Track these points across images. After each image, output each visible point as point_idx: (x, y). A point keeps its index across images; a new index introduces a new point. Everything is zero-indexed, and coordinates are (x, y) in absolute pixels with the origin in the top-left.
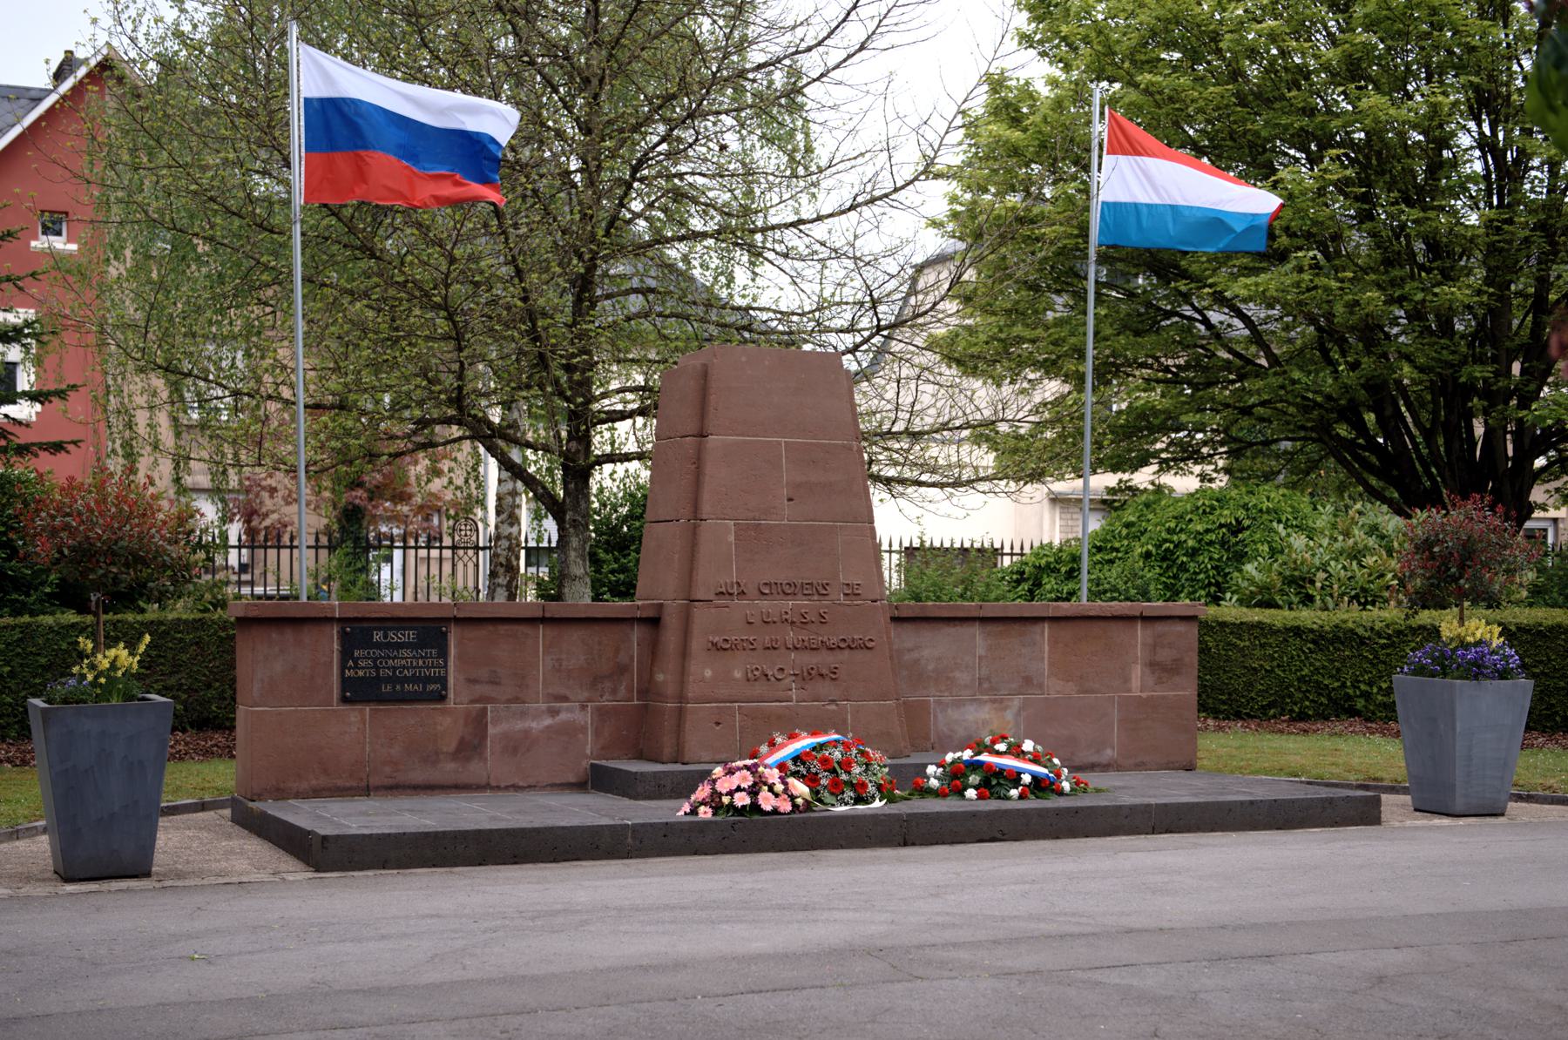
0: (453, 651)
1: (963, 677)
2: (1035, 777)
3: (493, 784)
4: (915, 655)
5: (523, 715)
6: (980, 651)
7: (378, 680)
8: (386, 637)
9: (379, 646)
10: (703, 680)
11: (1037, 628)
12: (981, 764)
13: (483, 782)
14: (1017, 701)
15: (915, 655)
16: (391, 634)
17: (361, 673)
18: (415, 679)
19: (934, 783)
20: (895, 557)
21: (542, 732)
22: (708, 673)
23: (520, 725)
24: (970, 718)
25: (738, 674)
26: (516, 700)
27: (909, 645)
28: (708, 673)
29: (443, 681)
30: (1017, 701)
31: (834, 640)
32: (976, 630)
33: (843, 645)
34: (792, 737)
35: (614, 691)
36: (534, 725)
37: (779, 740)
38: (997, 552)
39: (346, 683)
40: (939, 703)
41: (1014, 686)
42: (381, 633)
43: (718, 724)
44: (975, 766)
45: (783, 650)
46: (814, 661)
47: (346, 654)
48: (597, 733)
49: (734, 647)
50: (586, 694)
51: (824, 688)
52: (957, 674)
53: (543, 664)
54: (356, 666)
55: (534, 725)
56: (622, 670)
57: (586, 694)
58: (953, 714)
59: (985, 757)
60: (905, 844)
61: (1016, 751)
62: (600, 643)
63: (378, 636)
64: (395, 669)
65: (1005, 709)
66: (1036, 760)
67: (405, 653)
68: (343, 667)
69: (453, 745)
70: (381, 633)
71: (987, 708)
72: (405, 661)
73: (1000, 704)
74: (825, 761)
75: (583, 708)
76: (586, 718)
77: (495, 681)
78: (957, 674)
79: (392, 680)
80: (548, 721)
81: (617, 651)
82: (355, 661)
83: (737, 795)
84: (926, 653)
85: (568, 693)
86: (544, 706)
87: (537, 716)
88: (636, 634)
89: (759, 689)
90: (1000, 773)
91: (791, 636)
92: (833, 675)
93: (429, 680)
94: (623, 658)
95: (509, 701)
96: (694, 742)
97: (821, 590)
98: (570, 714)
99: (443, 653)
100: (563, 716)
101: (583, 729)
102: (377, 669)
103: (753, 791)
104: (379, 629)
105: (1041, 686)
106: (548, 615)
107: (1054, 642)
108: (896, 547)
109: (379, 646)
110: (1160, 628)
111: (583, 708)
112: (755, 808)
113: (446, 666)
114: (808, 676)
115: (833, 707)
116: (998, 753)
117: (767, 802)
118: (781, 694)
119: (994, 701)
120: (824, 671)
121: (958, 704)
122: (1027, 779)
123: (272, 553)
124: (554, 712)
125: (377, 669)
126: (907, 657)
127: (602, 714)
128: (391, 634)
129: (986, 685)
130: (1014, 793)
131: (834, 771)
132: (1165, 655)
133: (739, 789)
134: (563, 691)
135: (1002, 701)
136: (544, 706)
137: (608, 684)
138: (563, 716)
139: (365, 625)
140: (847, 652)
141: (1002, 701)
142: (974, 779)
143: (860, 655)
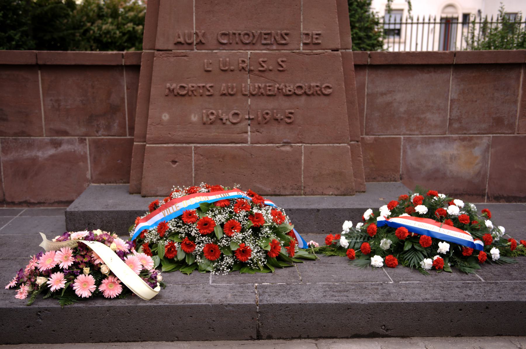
1: (434, 118)
2: (454, 245)
3: (9, 200)
4: (388, 98)
5: (30, 146)
6: (453, 95)
10: (161, 122)
11: (513, 74)
12: (397, 226)
14: (486, 140)
15: (388, 98)
19: (344, 242)
21: (47, 159)
22: (166, 117)
23: (28, 154)
24: (438, 153)
25: (194, 118)
26: (23, 133)
27: (382, 89)
28: (166, 117)
30: (486, 140)
31: (291, 87)
32: (450, 76)
33: (299, 92)
34: (191, 192)
35: (108, 127)
36: (40, 154)
37: (175, 195)
40: (409, 140)
41: (484, 126)
43: (174, 162)
44: (389, 228)
45: (239, 96)
48: (95, 161)
49: (190, 94)
50: (83, 130)
51: (278, 131)
52: (428, 115)
53: (44, 105)
55: (40, 154)
56: (114, 110)
57: (83, 130)
58: (422, 150)
59: (404, 220)
60: (259, 337)
61: (436, 214)
62: (93, 87)
65: (474, 146)
66: (457, 223)
71: (456, 145)
73: (468, 141)
74: (206, 224)
76: (85, 149)
78: (428, 115)
80: (52, 151)
83: (54, 276)
84: (398, 97)
85: (68, 129)
86: (47, 139)
87: (42, 147)
88: (125, 79)
89: (214, 132)
90: (416, 236)
91: (249, 84)
92: (288, 120)
95: (16, 134)
96: (150, 178)
98: (70, 146)
100: (65, 147)
101: (83, 158)
103: (71, 274)
105: (511, 126)
106: (40, 62)
111: (82, 141)
112: (69, 292)
114: (262, 121)
115: (288, 148)
116: (419, 216)
117: (84, 285)
118: (235, 136)
119: (463, 139)
120: (279, 116)
121: (428, 141)
122: (444, 247)
123: (409, 26)
124: (57, 144)
126: (380, 100)
127: (97, 145)
129: (456, 125)
130: (427, 263)
131: (213, 235)
133: (57, 269)
134: (63, 127)
135: (471, 139)
136: (47, 139)
137: (102, 122)
138: (65, 147)
140: (303, 98)
141: (471, 139)
142: (386, 243)
143: (316, 101)
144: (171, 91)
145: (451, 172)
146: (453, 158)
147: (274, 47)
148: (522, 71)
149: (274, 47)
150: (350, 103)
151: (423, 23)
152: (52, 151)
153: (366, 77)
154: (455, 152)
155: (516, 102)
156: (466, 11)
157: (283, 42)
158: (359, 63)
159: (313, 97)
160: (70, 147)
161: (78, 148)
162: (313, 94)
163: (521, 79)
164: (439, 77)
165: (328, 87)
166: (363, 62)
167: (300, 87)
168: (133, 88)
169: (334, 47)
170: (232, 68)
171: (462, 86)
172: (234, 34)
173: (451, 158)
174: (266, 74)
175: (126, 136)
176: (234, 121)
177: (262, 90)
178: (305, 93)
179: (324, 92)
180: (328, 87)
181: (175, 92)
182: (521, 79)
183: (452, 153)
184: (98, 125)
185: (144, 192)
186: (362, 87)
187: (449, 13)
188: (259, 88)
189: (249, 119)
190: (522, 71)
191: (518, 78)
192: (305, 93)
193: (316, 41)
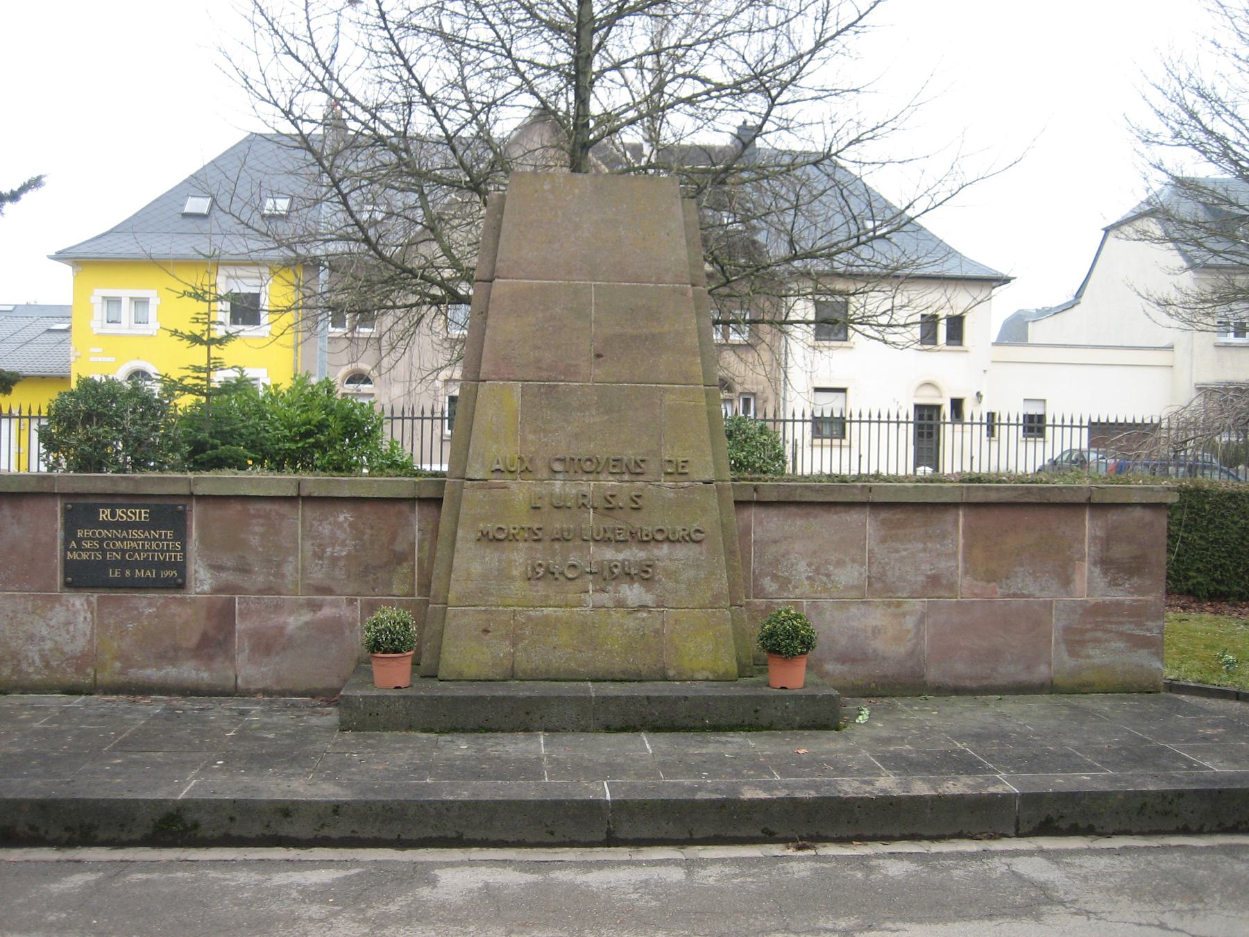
0: (194, 533)
7: (105, 565)
8: (113, 515)
9: (106, 525)
11: (948, 517)
13: (1083, 500)
16: (119, 512)
17: (85, 556)
18: (146, 565)
20: (1085, 431)
26: (269, 590)
29: (181, 567)
33: (659, 537)
38: (1155, 427)
39: (69, 566)
42: (108, 511)
46: (621, 557)
47: (70, 534)
54: (80, 548)
63: (104, 515)
64: (123, 551)
67: (134, 533)
68: (66, 548)
69: (194, 639)
70: (108, 511)
72: (142, 544)
75: (351, 602)
77: (244, 569)
79: (122, 564)
80: (306, 617)
81: (393, 539)
82: (79, 542)
88: (417, 520)
93: (162, 565)
94: (400, 546)
95: (261, 592)
97: (635, 470)
99: (181, 535)
100: (327, 612)
102: (104, 552)
104: (106, 506)
105: (951, 587)
106: (304, 493)
107: (970, 532)
108: (1085, 423)
109: (106, 525)
110: (1114, 517)
113: (184, 550)
114: (542, 574)
119: (889, 605)
124: (315, 607)
125: (104, 552)
128: (119, 512)
132: (1120, 551)
135: (899, 605)
136: (302, 599)
139: (91, 501)
144: (485, 535)
145: (874, 651)
146: (876, 631)
147: (626, 477)
148: (961, 513)
149: (626, 477)
150: (730, 553)
151: (870, 422)
152: (306, 617)
153: (752, 514)
154: (879, 623)
155: (955, 554)
156: (957, 396)
157: (638, 470)
158: (740, 499)
159: (678, 545)
160: (334, 610)
161: (345, 612)
162: (678, 541)
163: (961, 524)
164: (854, 517)
165: (698, 531)
166: (745, 497)
167: (661, 531)
168: (434, 533)
169: (707, 478)
170: (569, 504)
171: (883, 533)
172: (572, 459)
173: (873, 632)
174: (615, 513)
175: (413, 595)
176: (570, 576)
177: (609, 535)
178: (668, 539)
179: (693, 537)
180: (698, 531)
181: (491, 536)
182: (961, 524)
183: (874, 623)
184: (374, 580)
185: (440, 677)
186: (746, 532)
187: (928, 398)
188: (582, 758)
189: (591, 573)
190: (961, 513)
191: (956, 522)
192: (668, 539)
193: (680, 470)
